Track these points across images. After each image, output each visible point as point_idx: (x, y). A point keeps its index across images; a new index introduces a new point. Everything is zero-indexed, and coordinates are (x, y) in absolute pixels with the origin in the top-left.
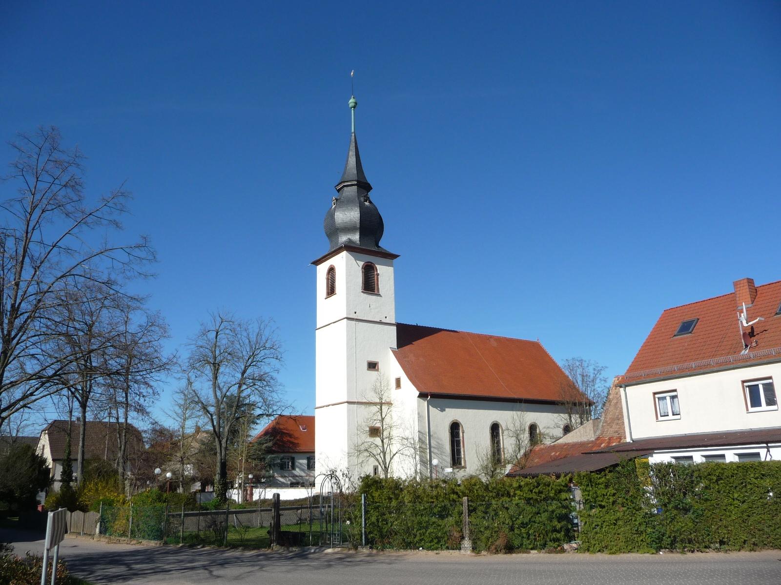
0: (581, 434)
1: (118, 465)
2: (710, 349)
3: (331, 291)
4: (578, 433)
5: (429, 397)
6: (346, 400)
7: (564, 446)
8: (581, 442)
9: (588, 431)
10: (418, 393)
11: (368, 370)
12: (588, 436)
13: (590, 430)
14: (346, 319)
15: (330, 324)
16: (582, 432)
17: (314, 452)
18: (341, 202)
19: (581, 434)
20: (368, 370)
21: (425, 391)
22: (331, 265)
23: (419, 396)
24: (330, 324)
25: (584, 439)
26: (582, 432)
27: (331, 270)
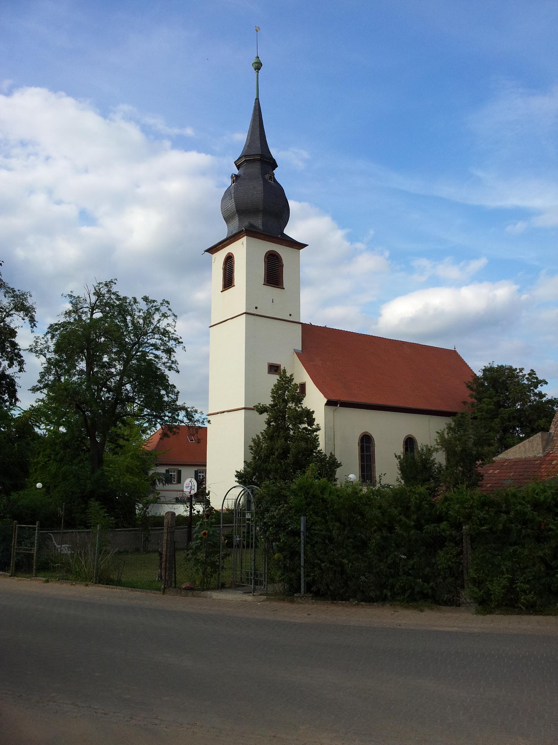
0: (526, 449)
1: (91, 550)
2: (507, 475)
3: (228, 282)
4: (522, 448)
5: (339, 405)
6: (243, 406)
7: (504, 462)
8: (525, 458)
9: (535, 445)
10: (325, 400)
11: (269, 373)
12: (535, 452)
13: (538, 444)
14: (245, 314)
15: (224, 412)
16: (527, 447)
17: (206, 466)
18: (241, 179)
19: (526, 449)
20: (269, 373)
21: (334, 398)
22: (229, 253)
23: (326, 404)
24: (224, 412)
25: (530, 455)
26: (527, 447)
27: (229, 260)
